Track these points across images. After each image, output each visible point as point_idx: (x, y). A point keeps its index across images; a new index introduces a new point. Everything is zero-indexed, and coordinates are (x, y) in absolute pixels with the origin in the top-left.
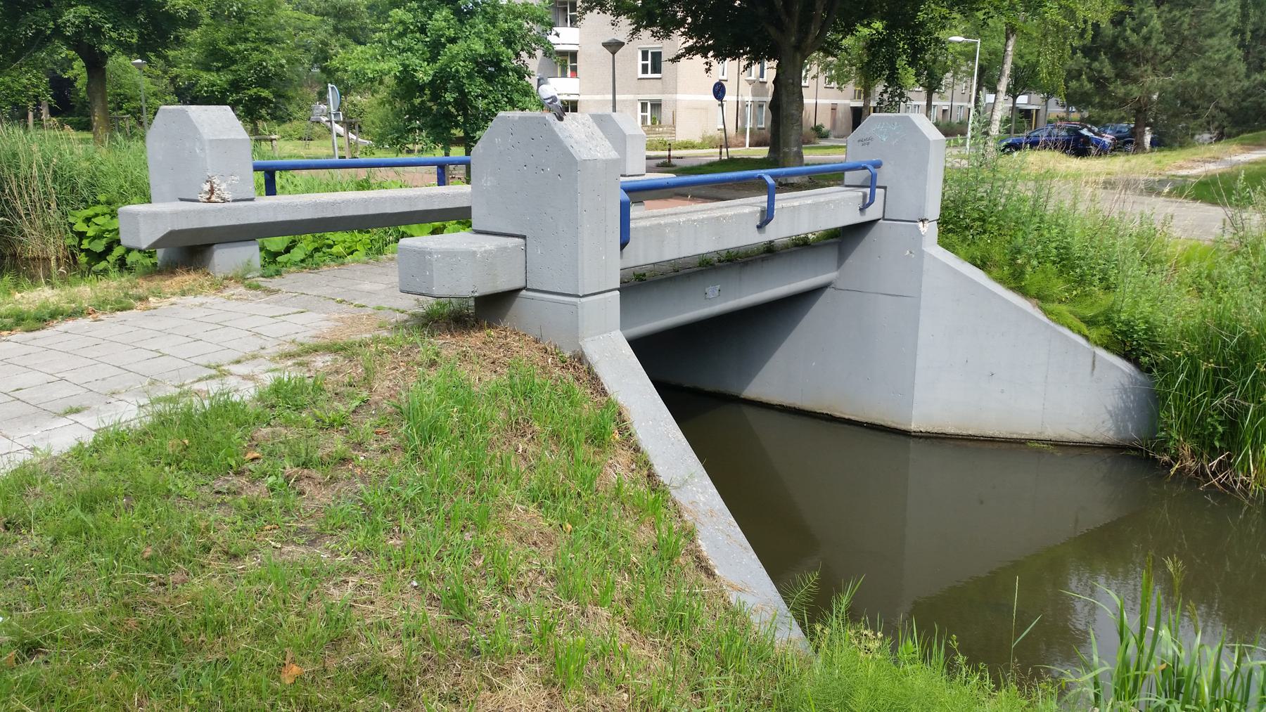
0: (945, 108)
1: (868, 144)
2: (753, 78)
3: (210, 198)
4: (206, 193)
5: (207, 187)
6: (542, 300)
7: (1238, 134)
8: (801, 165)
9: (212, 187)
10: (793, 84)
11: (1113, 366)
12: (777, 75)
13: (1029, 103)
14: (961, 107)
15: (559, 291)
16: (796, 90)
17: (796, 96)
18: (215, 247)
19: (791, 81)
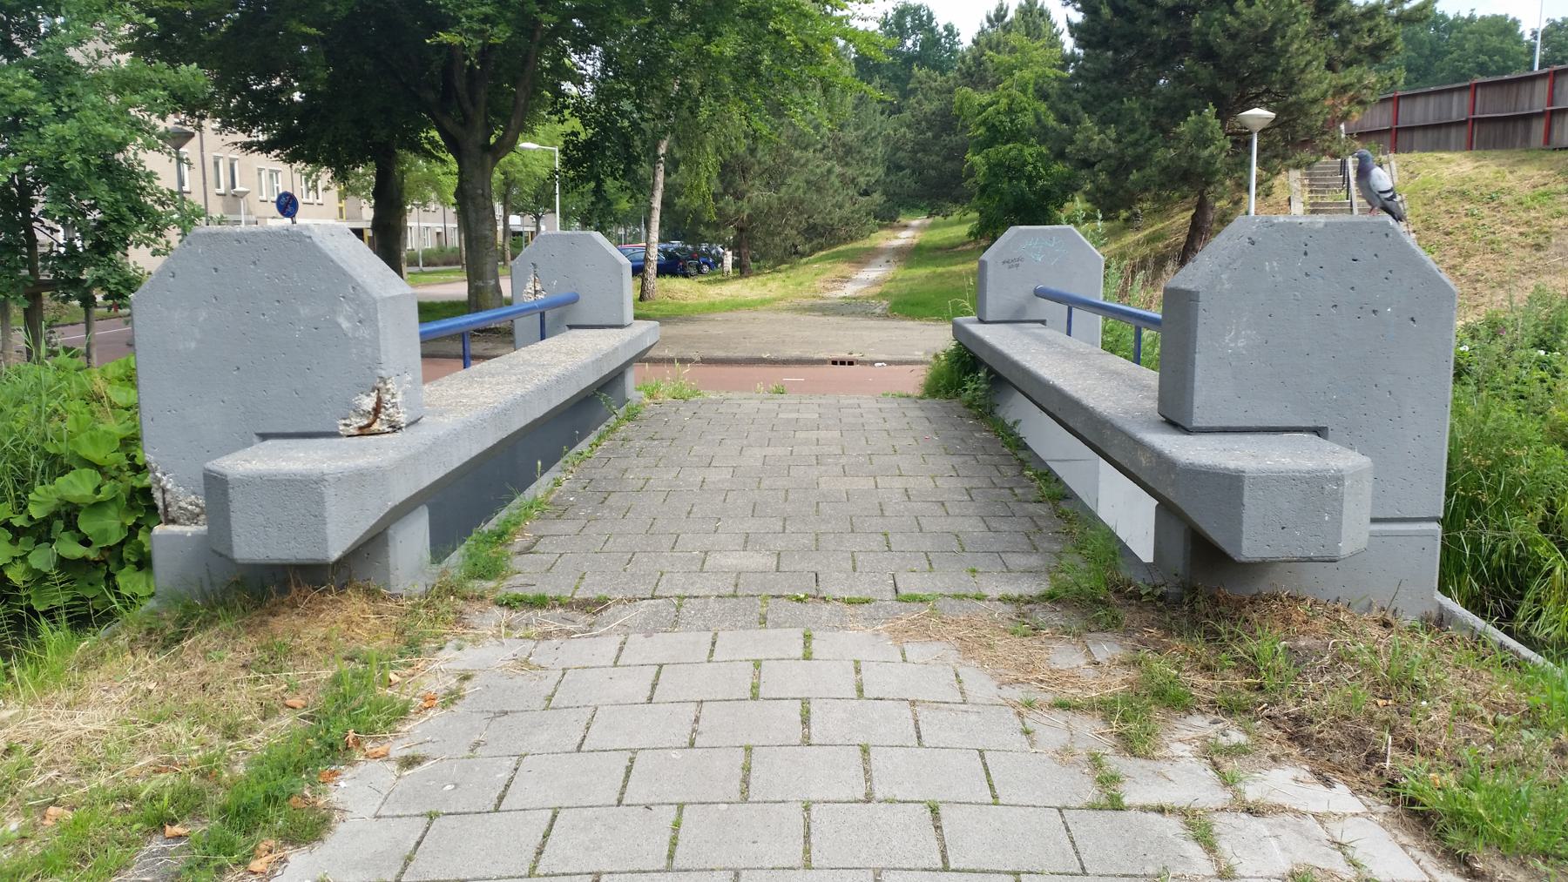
0: (439, 230)
1: (1017, 266)
2: (222, 190)
3: (369, 425)
4: (365, 414)
5: (368, 403)
6: (1397, 535)
7: (812, 252)
8: (501, 306)
9: (379, 400)
10: (483, 195)
11: (1439, 505)
12: (461, 181)
13: (522, 225)
14: (427, 228)
15: (1398, 515)
16: (488, 204)
17: (487, 212)
18: (390, 532)
19: (480, 191)
